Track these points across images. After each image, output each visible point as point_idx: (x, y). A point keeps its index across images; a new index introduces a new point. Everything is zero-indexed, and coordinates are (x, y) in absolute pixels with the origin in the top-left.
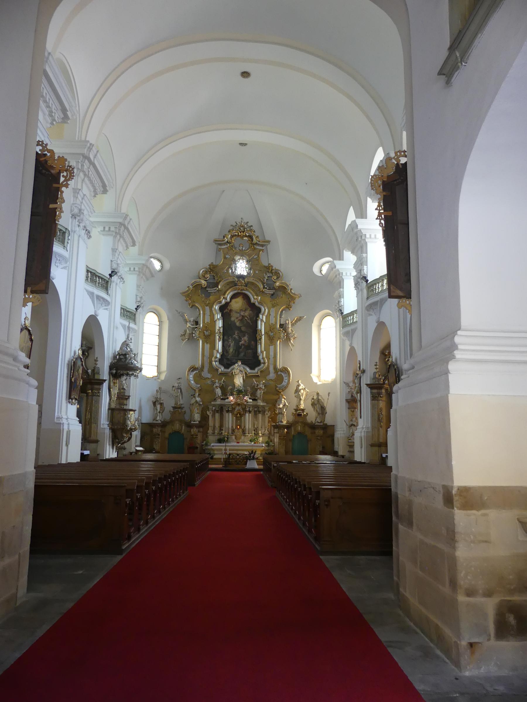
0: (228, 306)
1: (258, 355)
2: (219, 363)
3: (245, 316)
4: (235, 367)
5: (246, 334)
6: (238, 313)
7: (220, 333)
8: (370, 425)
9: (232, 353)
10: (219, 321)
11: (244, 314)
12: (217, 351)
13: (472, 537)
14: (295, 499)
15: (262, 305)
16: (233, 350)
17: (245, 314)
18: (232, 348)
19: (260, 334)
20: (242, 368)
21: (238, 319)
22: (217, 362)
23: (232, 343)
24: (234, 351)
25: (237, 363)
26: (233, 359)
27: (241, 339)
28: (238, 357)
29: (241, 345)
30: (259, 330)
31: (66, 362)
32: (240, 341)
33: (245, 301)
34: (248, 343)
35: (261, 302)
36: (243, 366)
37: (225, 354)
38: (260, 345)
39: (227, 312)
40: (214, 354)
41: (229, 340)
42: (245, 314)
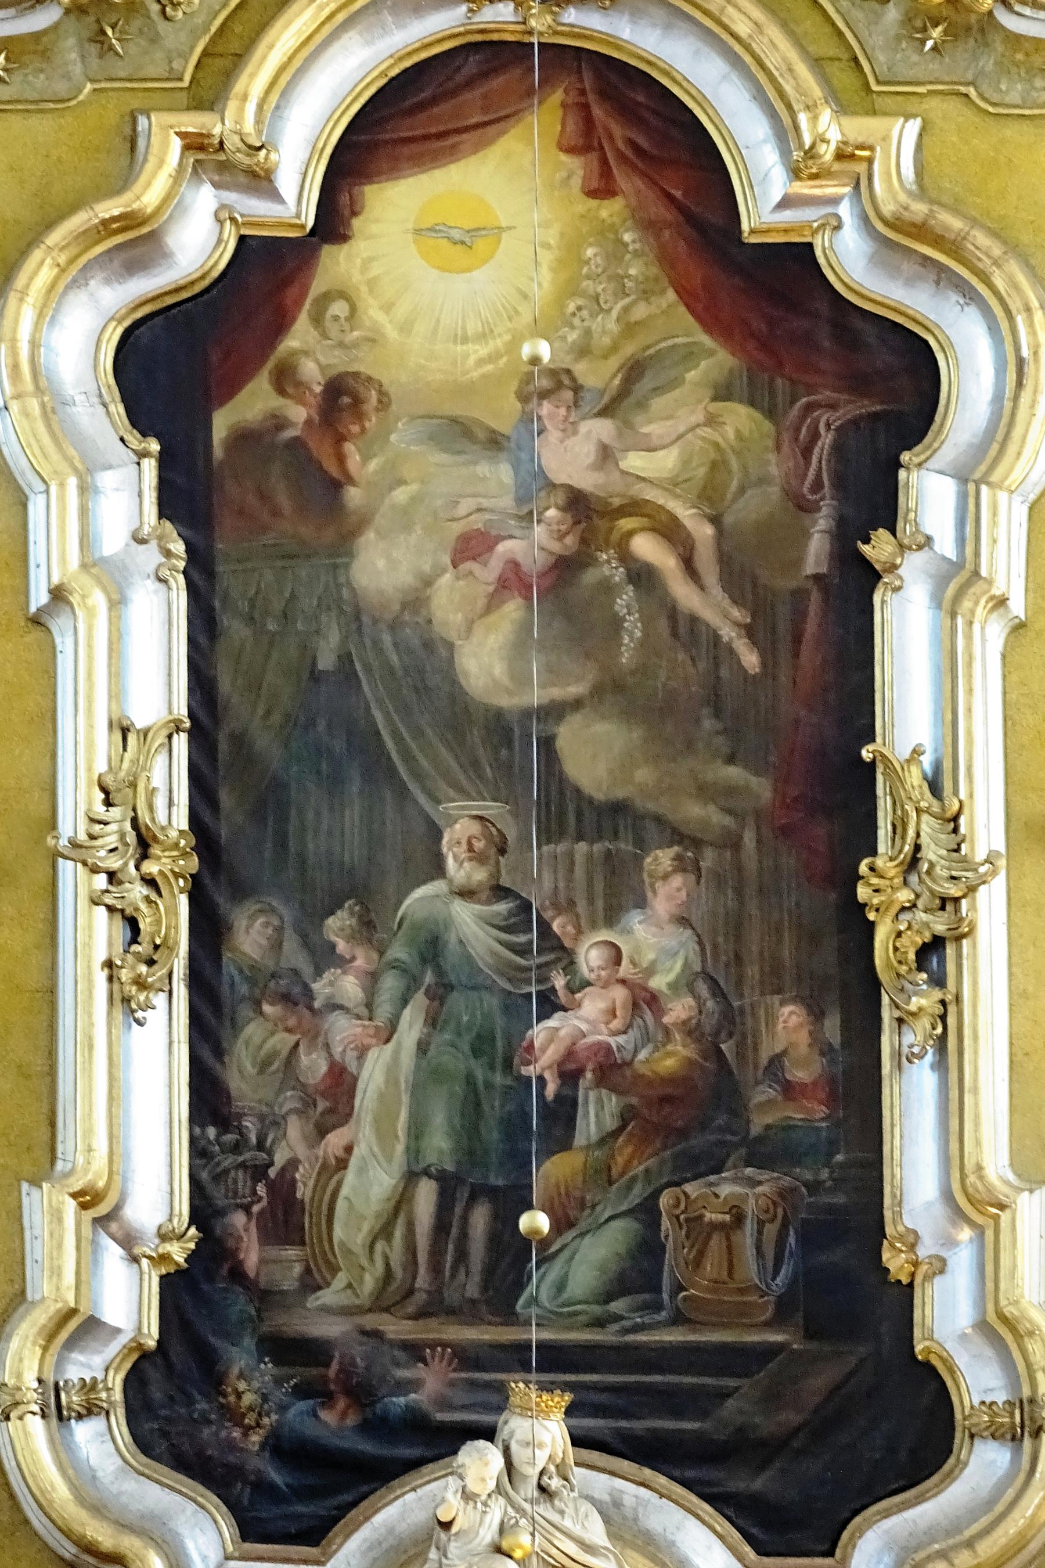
0: (281, 325)
1: (895, 1261)
2: (143, 1443)
3: (634, 507)
4: (452, 1507)
5: (663, 858)
6: (495, 442)
7: (144, 844)
8: (1030, 1346)
9: (385, 1231)
10: (117, 603)
11: (606, 455)
12: (87, 1198)
13: (295, 769)
14: (640, 104)
15: (944, 278)
16: (411, 1177)
17: (634, 462)
18: (384, 1134)
19: (931, 853)
20: (596, 1532)
21: (489, 571)
22: (89, 1411)
23: (388, 1033)
24: (426, 1194)
25: (489, 1434)
26: (415, 1351)
27: (566, 958)
28: (508, 1316)
29: (569, 1076)
30: (914, 778)
31: (381, 1328)
32: (549, 1004)
33: (610, 210)
34: (691, 1030)
35: (921, 231)
36: (601, 1484)
37: (251, 1256)
38: (882, 590)
39: (279, 422)
40: (36, 1250)
41: (321, 988)
42: (634, 462)
